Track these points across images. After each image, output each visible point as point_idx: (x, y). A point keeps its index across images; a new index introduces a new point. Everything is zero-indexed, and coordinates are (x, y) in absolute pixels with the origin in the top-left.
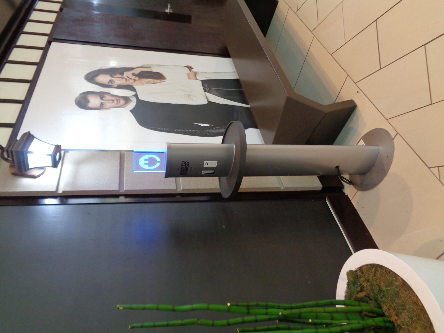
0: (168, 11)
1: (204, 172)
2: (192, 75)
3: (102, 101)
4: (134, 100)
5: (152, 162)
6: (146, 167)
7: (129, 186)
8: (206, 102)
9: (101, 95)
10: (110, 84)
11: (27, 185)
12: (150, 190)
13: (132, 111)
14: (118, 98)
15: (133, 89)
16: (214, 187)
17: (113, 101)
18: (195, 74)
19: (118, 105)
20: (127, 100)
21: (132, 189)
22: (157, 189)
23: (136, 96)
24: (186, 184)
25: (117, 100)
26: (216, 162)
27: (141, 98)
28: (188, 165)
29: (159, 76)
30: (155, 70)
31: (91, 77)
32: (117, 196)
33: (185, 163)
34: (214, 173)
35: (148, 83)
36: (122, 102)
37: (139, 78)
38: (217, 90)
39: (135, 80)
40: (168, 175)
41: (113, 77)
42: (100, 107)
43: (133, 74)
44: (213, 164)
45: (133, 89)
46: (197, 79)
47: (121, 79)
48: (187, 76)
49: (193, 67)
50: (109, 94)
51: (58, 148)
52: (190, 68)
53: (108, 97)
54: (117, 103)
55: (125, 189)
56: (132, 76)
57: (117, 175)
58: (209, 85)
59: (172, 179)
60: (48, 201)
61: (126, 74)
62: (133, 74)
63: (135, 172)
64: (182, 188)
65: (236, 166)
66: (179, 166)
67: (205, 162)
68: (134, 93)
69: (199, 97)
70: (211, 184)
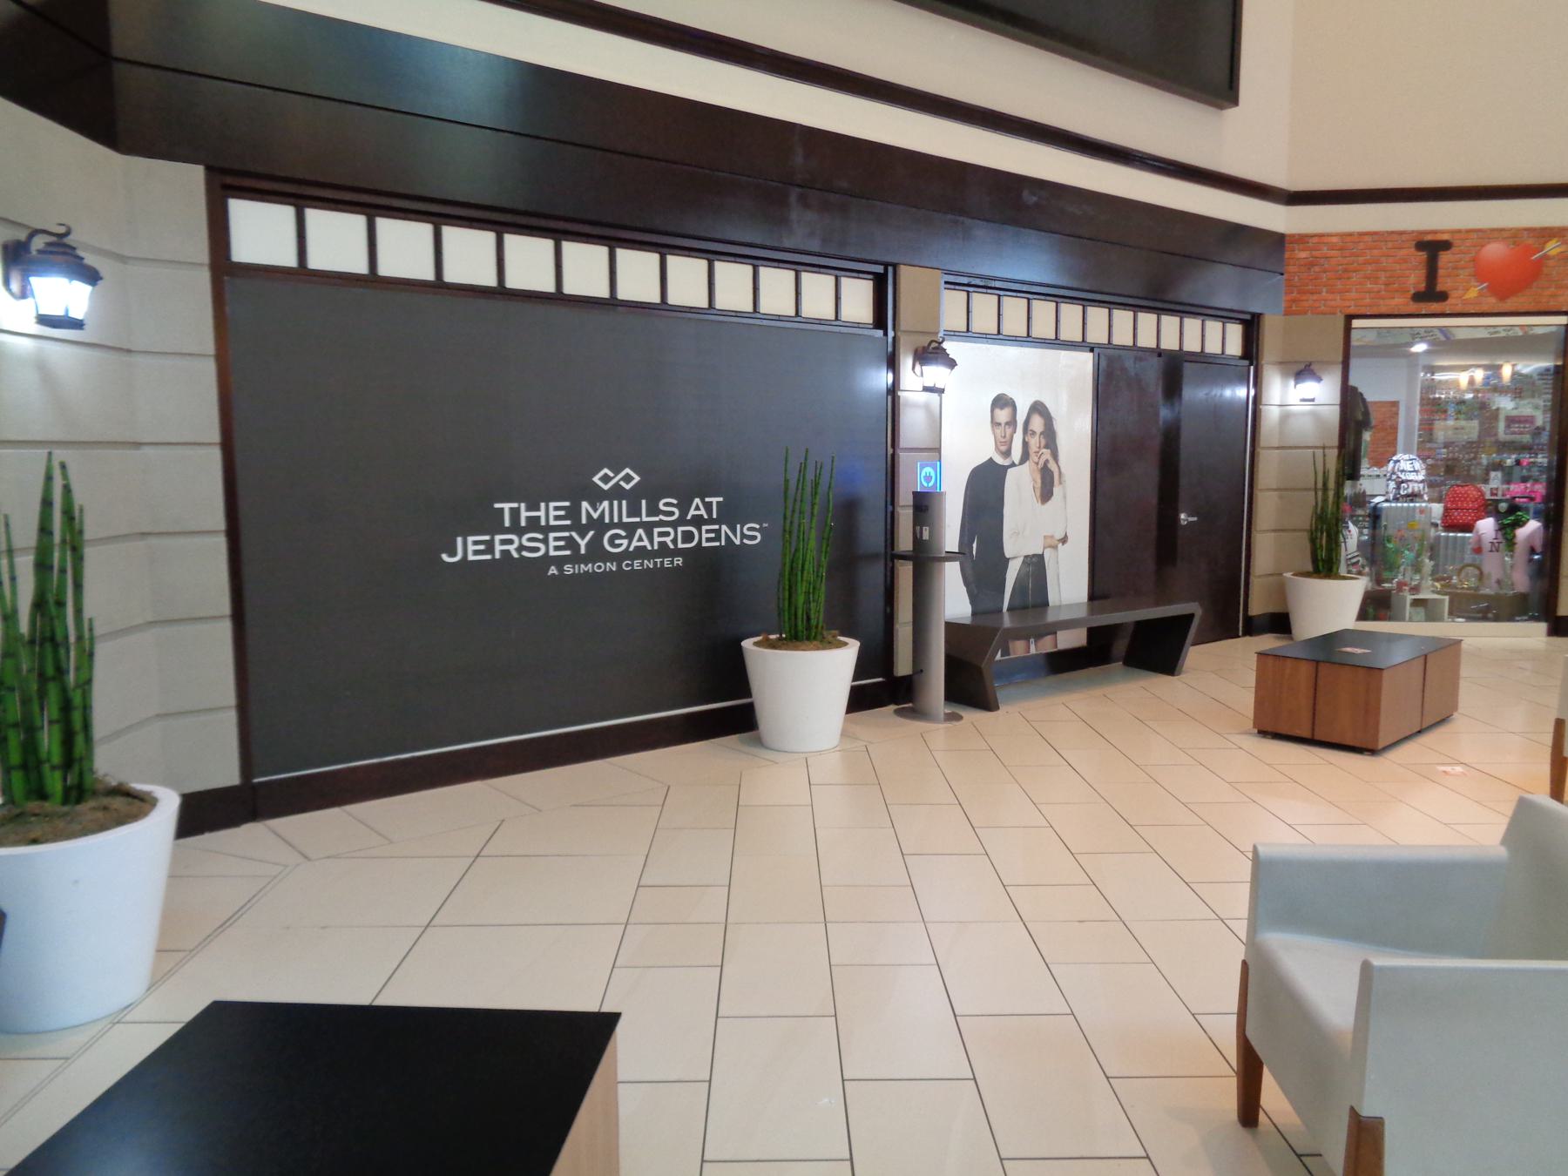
0: (1183, 516)
2: (1049, 541)
4: (1006, 463)
5: (928, 479)
7: (903, 457)
11: (906, 362)
15: (1022, 462)
18: (1055, 547)
20: (1007, 454)
23: (1013, 465)
24: (905, 516)
29: (1046, 494)
31: (1038, 408)
34: (917, 541)
36: (1003, 448)
38: (1027, 574)
40: (916, 495)
44: (926, 536)
45: (1022, 462)
51: (942, 391)
52: (1064, 540)
53: (1009, 431)
58: (1036, 566)
59: (911, 502)
60: (890, 376)
65: (924, 559)
66: (924, 505)
69: (1018, 543)
70: (905, 543)
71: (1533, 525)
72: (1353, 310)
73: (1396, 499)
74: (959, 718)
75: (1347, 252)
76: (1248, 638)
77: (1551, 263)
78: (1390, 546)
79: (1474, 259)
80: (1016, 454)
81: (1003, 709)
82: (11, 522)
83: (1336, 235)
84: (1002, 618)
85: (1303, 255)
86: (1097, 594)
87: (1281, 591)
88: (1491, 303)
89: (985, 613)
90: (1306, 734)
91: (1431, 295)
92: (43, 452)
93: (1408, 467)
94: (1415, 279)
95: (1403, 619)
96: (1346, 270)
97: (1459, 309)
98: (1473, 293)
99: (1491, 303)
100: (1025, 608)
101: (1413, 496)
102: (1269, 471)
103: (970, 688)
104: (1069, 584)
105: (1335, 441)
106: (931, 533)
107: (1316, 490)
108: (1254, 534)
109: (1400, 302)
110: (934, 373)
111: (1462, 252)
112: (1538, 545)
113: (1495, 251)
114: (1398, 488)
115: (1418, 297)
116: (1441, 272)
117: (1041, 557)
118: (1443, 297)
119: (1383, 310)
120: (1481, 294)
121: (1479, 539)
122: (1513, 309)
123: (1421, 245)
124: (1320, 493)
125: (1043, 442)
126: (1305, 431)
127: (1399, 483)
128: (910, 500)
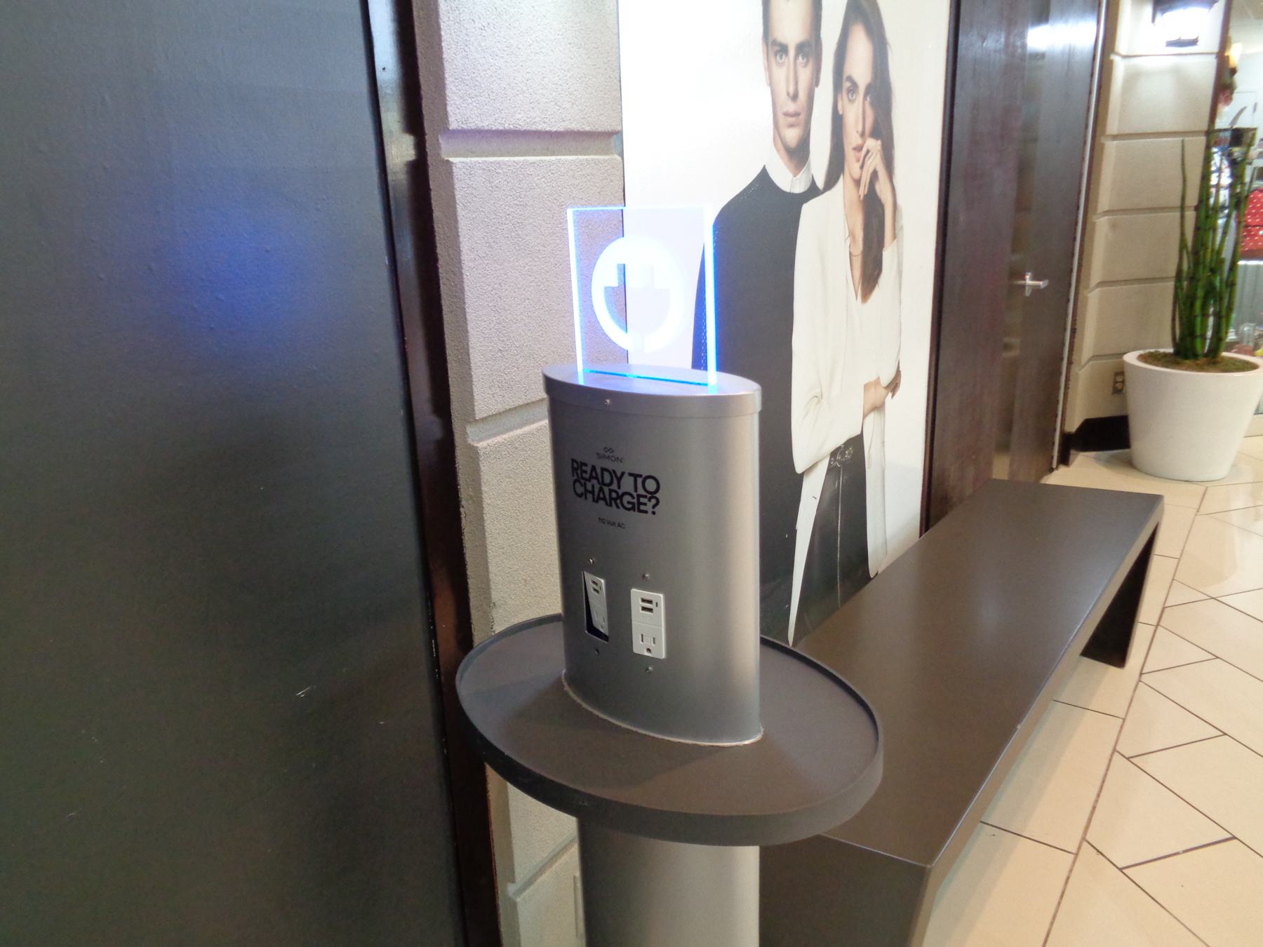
0: (1029, 281)
1: (597, 587)
2: (875, 396)
3: (792, 52)
6: (604, 276)
7: (470, 180)
8: (799, 469)
9: (810, 48)
10: (847, 84)
12: (462, 290)
13: (764, 177)
14: (802, 117)
16: (495, 596)
17: (795, 97)
19: (783, 121)
20: (798, 155)
21: (459, 195)
22: (470, 326)
23: (813, 192)
25: (796, 114)
26: (661, 652)
27: (808, 209)
28: (637, 507)
29: (870, 273)
30: (888, 255)
32: (414, 122)
33: (653, 495)
35: (852, 234)
36: (792, 136)
37: (865, 196)
39: (857, 182)
40: (564, 400)
41: (866, 94)
42: (775, 43)
43: (875, 175)
44: (649, 633)
45: (831, 182)
46: (865, 416)
47: (860, 128)
48: (873, 378)
49: (898, 394)
50: (815, 80)
52: (894, 386)
53: (805, 74)
54: (787, 114)
55: (460, 163)
56: (871, 170)
57: (520, 120)
58: (849, 465)
61: (873, 145)
62: (875, 175)
63: (570, 213)
64: (481, 445)
67: (660, 597)
68: (820, 184)
82: (1174, 38)
87: (1118, 381)
92: (1179, 139)
124: (1191, 215)
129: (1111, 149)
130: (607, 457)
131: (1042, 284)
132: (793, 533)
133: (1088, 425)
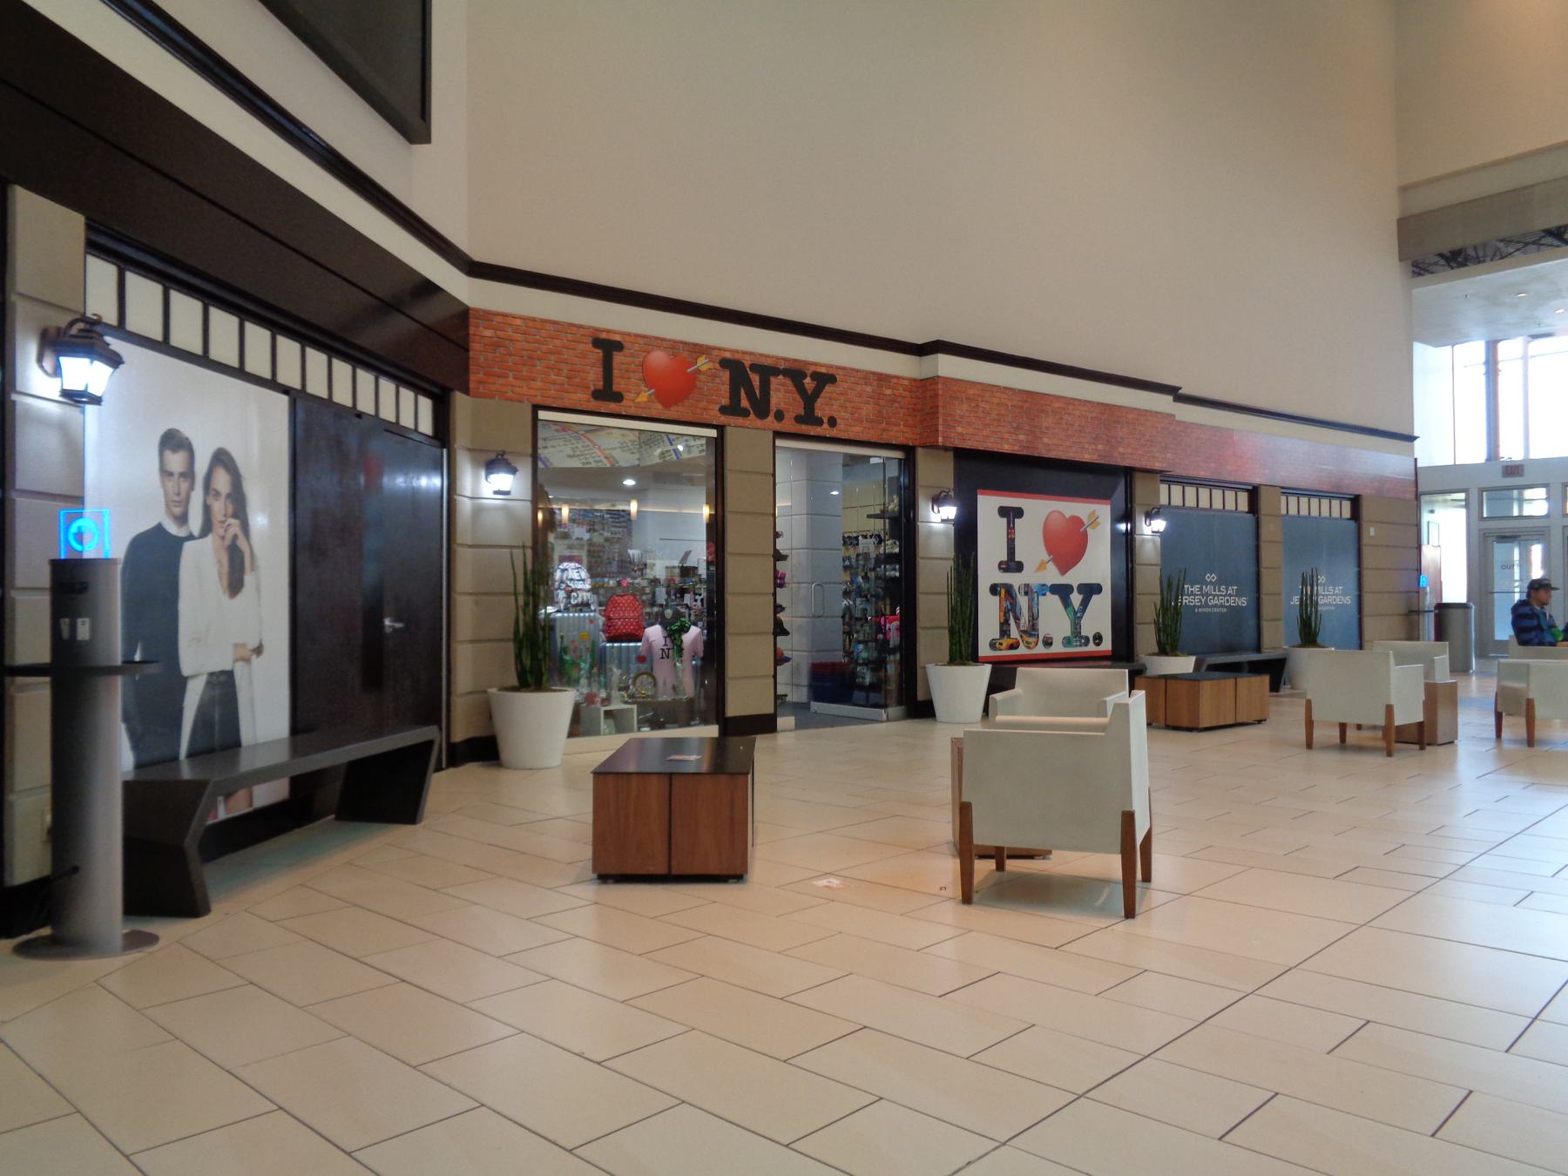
0: (387, 622)
6: (74, 529)
18: (247, 660)
20: (182, 519)
23: (191, 537)
29: (235, 585)
31: (221, 458)
36: (178, 511)
40: (58, 567)
50: (192, 488)
58: (223, 687)
62: (235, 537)
69: (198, 658)
71: (694, 631)
72: (539, 400)
73: (567, 609)
74: (152, 939)
75: (531, 338)
76: (451, 770)
77: (702, 377)
78: (567, 658)
79: (642, 364)
80: (195, 523)
81: (218, 909)
83: (521, 318)
84: (178, 769)
85: (488, 333)
86: (300, 725)
88: (657, 409)
89: (153, 763)
90: (661, 869)
91: (607, 396)
93: (576, 576)
94: (594, 377)
95: (598, 733)
96: (530, 357)
97: (632, 411)
98: (643, 397)
99: (657, 409)
100: (211, 751)
101: (585, 605)
102: (465, 578)
103: (165, 886)
104: (266, 716)
105: (529, 543)
106: (93, 630)
107: (515, 594)
108: (453, 645)
109: (581, 398)
110: (82, 372)
111: (632, 355)
112: (701, 648)
113: (658, 358)
114: (569, 597)
115: (597, 395)
116: (616, 372)
117: (229, 675)
118: (618, 398)
119: (567, 404)
120: (650, 400)
121: (650, 646)
122: (675, 417)
123: (598, 343)
125: (230, 509)
126: (499, 529)
127: (569, 593)
128: (44, 578)
129: (464, 558)
130: (71, 581)
131: (399, 625)
132: (181, 710)
133: (470, 742)
